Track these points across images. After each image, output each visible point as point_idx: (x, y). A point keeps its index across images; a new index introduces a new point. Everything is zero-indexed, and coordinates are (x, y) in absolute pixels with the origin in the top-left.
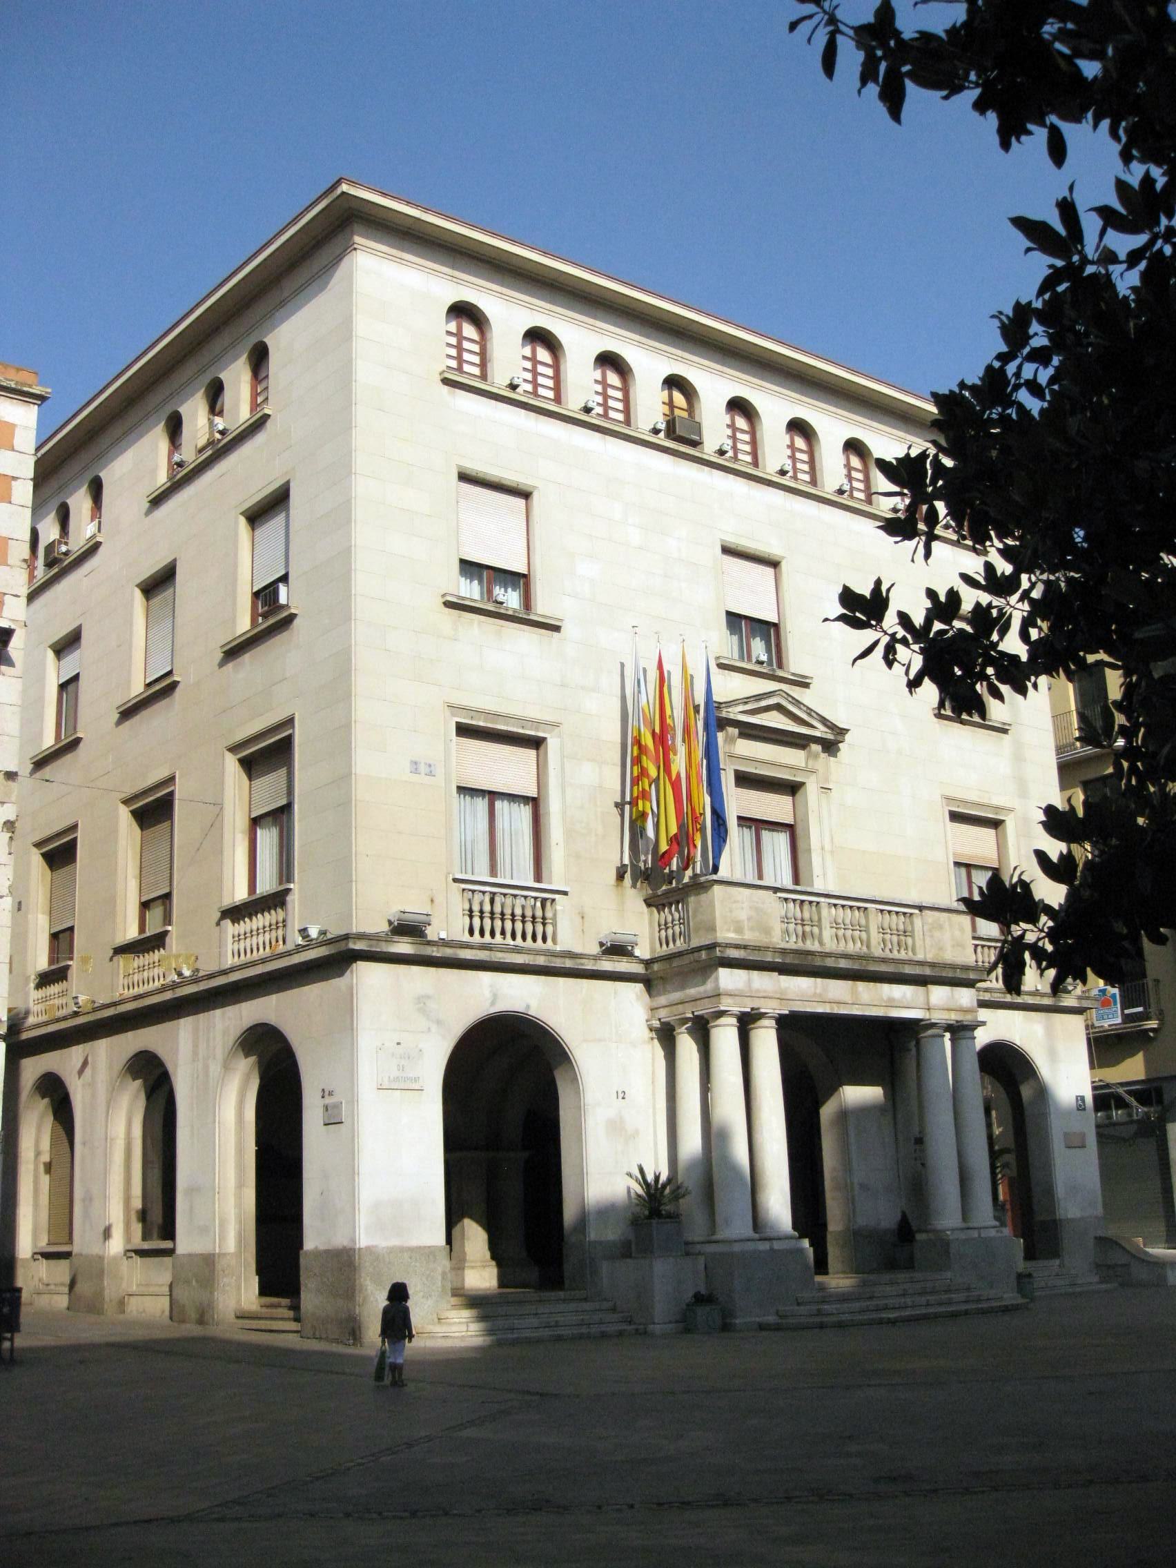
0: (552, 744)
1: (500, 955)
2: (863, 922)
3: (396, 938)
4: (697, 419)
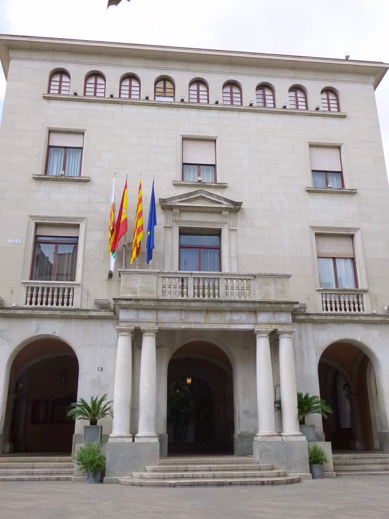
1: (37, 311)
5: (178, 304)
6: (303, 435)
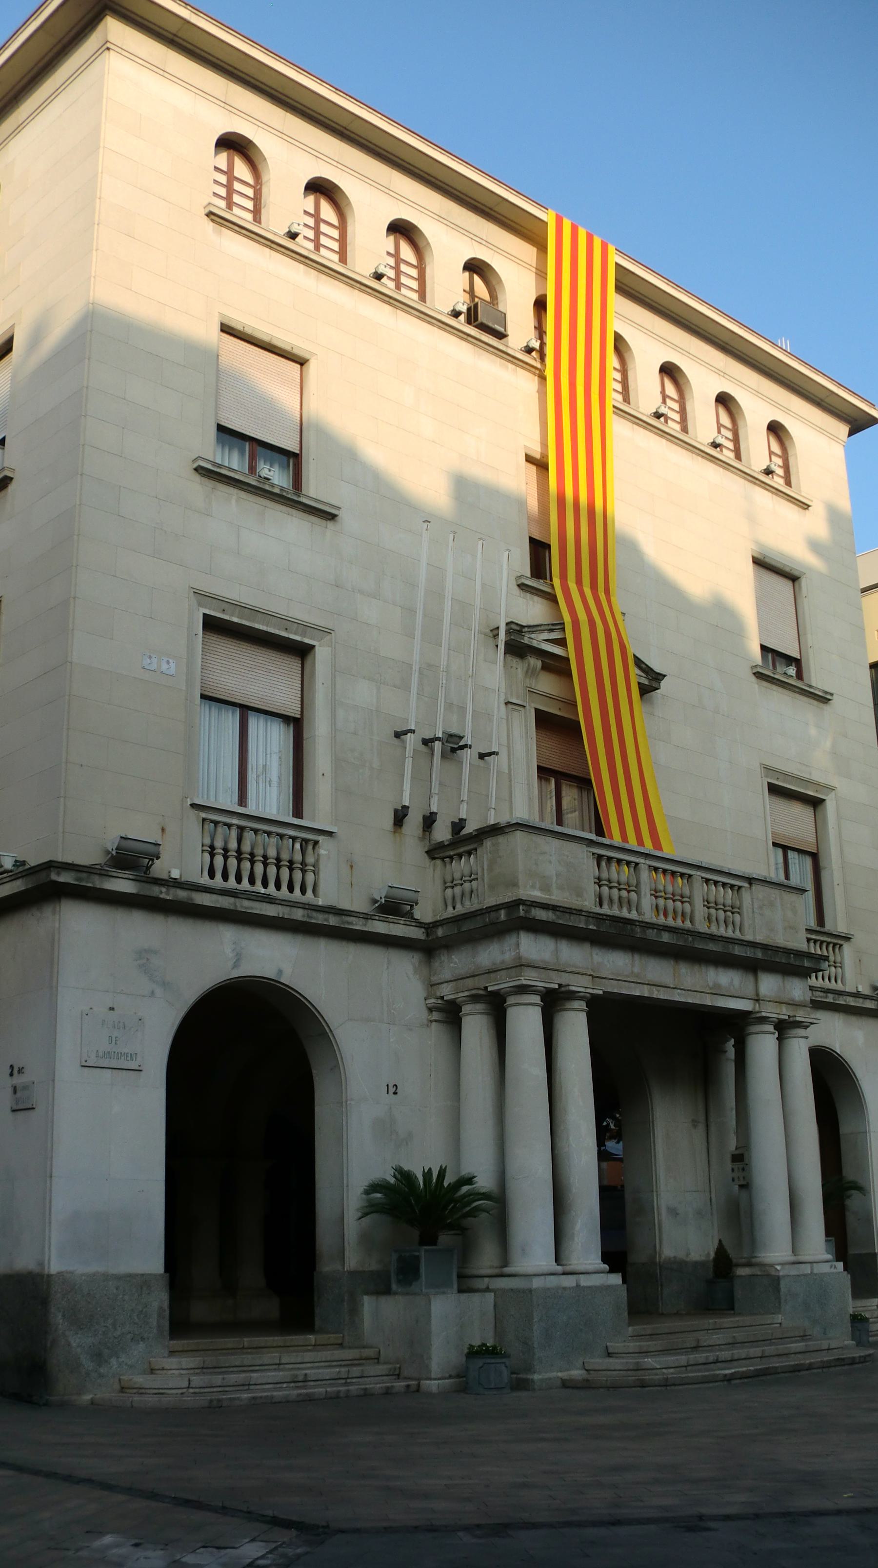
0: (322, 654)
1: (246, 903)
2: (687, 891)
3: (114, 872)
4: (501, 308)
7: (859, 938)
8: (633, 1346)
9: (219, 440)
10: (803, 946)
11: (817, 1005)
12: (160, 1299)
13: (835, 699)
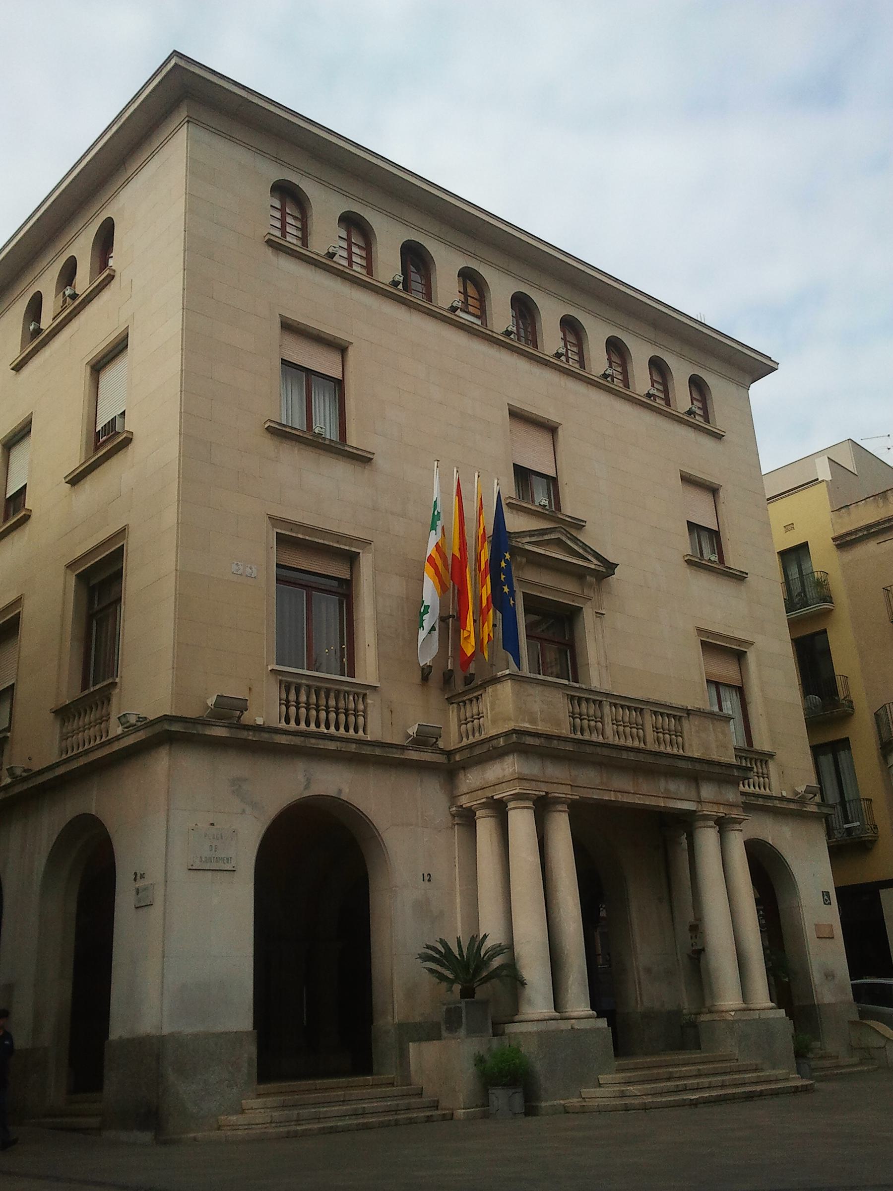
1: (313, 741)
2: (640, 721)
5: (632, 756)
6: (598, 1017)
7: (781, 755)
8: (620, 1076)
9: (284, 373)
10: (734, 761)
11: (748, 807)
12: (250, 1050)
13: (750, 578)
